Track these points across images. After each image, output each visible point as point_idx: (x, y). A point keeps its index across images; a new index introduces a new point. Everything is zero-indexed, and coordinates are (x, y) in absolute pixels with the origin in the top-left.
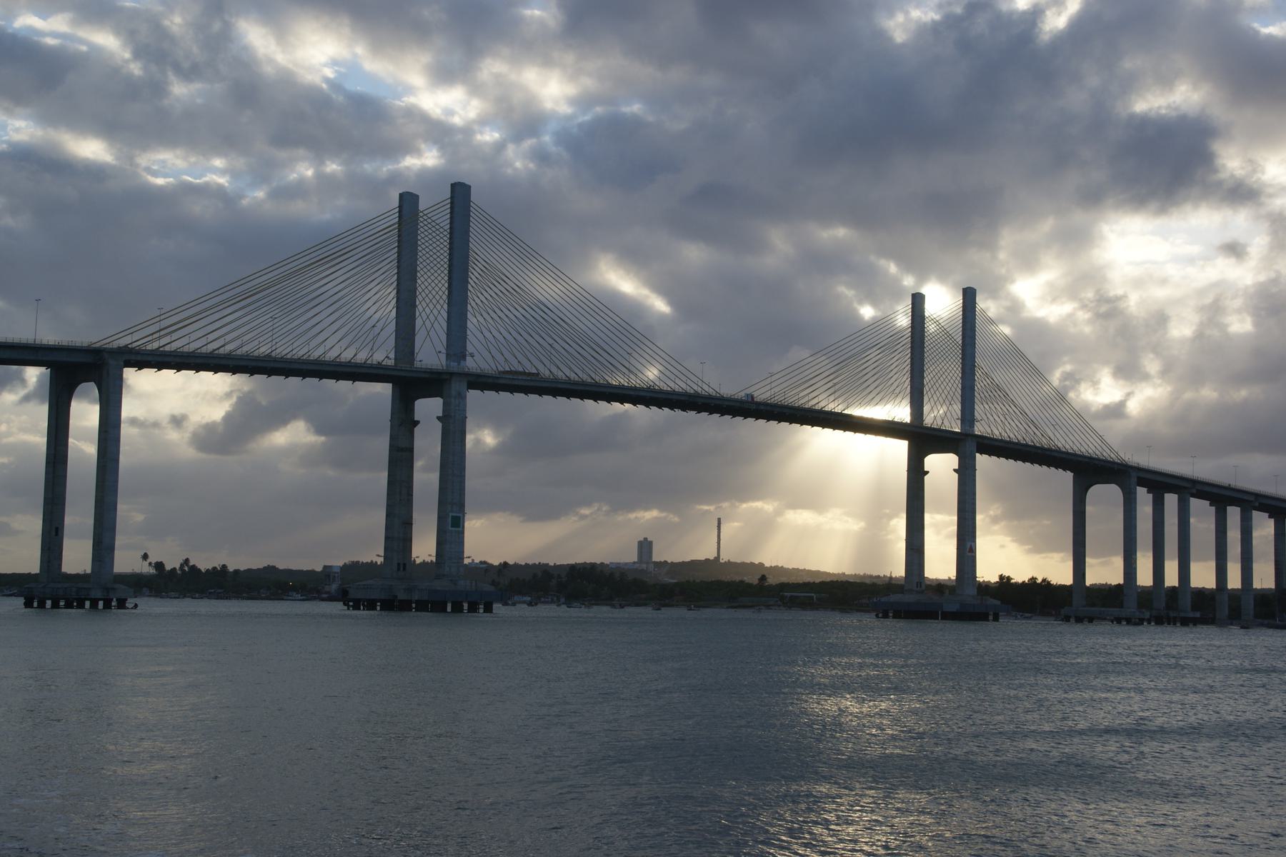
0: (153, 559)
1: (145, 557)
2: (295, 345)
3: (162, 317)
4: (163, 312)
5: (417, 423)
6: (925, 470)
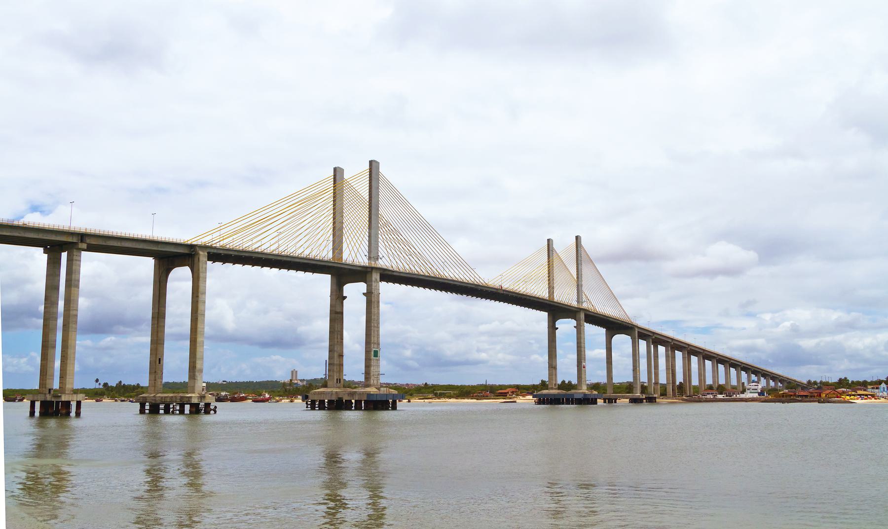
0: (102, 382)
1: (97, 381)
2: (244, 241)
3: (221, 228)
4: (222, 225)
5: (345, 297)
6: (556, 327)
